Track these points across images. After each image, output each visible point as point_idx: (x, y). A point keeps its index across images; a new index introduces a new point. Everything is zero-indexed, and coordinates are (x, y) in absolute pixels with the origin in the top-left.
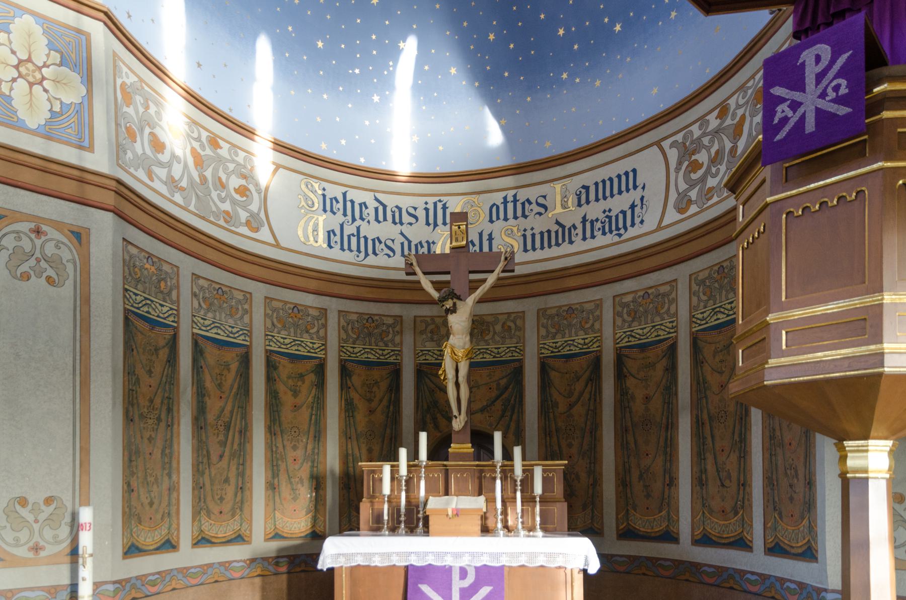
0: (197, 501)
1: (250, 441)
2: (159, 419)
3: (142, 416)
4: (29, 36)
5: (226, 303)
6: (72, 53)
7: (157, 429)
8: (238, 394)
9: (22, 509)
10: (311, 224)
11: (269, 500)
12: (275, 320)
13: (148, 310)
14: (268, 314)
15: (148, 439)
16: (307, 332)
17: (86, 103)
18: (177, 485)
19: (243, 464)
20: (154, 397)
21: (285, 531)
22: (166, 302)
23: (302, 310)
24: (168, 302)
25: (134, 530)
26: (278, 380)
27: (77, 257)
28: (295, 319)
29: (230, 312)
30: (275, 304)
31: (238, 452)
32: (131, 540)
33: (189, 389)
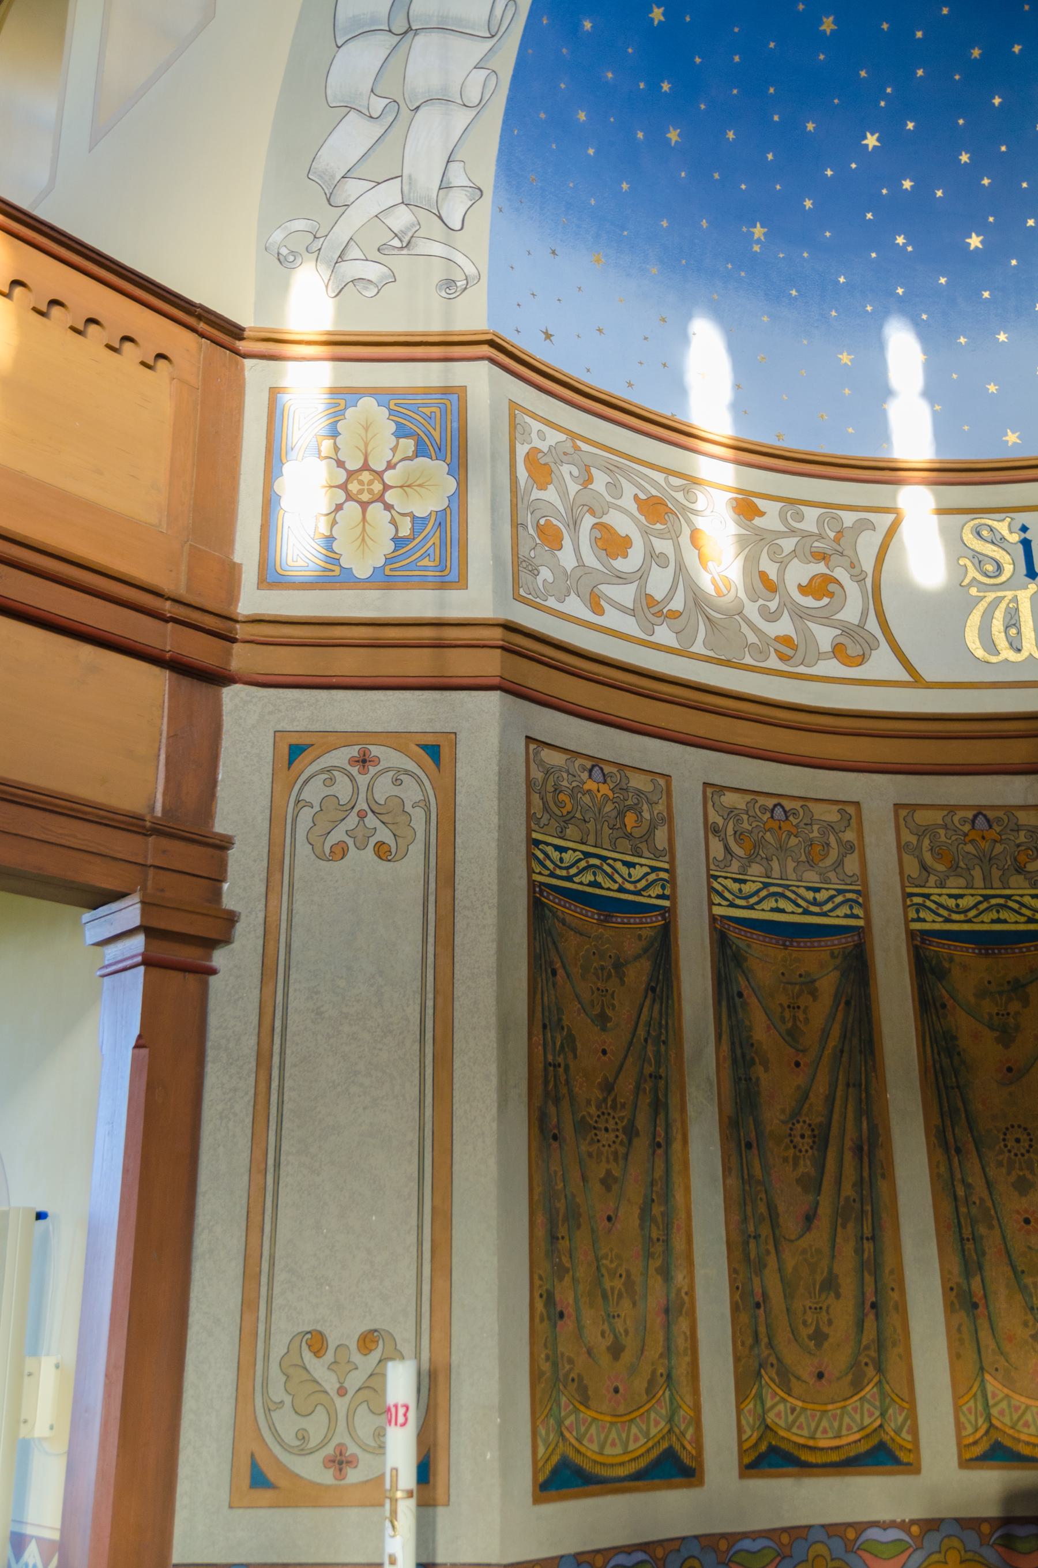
0: (750, 1341)
1: (887, 1172)
2: (631, 1132)
3: (582, 1127)
4: (367, 429)
5: (796, 836)
6: (435, 430)
7: (626, 1157)
8: (842, 1051)
9: (315, 1360)
10: (999, 614)
11: (961, 1341)
12: (928, 857)
13: (592, 879)
14: (908, 844)
15: (604, 1182)
16: (1020, 870)
17: (455, 507)
18: (686, 1298)
19: (873, 1238)
20: (616, 1078)
21: (1023, 1437)
22: (641, 857)
23: (999, 820)
24: (646, 853)
25: (567, 1423)
26: (950, 1003)
27: (431, 792)
28: (983, 844)
29: (808, 854)
30: (923, 818)
31: (857, 1205)
32: (559, 1451)
33: (710, 1049)
